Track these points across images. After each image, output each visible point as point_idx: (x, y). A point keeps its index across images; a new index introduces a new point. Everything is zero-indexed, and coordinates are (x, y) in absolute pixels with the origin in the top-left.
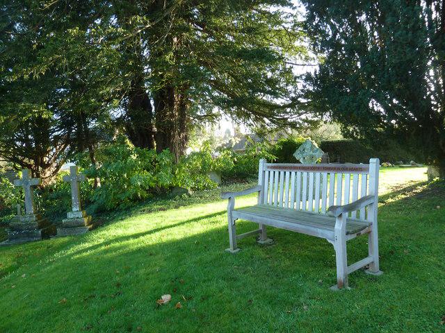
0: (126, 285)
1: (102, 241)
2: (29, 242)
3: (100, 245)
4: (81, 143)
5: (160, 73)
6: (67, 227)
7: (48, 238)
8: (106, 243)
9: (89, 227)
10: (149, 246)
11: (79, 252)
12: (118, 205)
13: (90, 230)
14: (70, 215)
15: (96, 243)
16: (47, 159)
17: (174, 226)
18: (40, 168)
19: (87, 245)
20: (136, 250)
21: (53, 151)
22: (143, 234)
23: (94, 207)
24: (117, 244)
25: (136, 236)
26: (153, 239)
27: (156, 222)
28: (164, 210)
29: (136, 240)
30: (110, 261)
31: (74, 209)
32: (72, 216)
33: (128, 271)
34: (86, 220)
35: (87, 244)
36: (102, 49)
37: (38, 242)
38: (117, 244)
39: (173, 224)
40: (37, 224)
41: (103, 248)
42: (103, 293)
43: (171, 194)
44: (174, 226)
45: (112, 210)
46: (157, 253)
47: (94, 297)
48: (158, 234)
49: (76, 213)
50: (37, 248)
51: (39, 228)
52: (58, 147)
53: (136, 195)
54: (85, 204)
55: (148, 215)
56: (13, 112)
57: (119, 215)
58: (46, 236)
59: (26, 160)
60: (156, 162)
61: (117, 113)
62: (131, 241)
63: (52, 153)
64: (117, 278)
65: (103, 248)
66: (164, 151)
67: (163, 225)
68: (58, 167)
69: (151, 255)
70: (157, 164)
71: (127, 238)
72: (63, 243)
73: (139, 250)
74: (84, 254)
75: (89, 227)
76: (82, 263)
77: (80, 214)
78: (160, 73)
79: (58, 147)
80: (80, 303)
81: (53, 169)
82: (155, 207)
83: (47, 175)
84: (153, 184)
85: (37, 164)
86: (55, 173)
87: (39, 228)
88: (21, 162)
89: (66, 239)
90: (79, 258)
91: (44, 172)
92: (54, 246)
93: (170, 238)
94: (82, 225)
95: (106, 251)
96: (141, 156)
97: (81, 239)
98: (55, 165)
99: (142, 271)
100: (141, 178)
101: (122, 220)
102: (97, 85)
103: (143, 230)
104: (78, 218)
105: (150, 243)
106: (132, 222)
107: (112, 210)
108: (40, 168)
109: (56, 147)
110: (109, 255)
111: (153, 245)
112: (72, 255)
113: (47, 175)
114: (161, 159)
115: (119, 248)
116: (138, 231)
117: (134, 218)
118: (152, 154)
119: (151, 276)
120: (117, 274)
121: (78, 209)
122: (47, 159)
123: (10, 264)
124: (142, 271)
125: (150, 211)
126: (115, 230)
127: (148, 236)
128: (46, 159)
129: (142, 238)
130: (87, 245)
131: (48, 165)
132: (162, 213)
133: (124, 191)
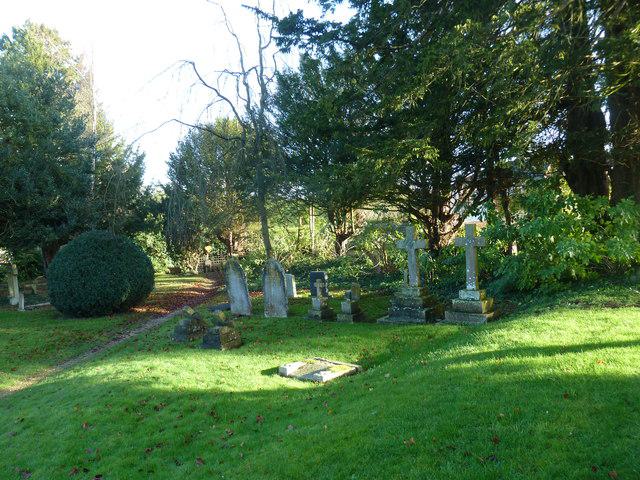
0: (508, 446)
1: (495, 347)
2: (411, 323)
3: (489, 355)
4: (493, 184)
5: (615, 64)
6: (457, 310)
7: (434, 322)
8: (500, 354)
9: (488, 316)
10: (568, 376)
11: (458, 360)
12: (538, 285)
13: (489, 320)
14: (463, 294)
15: (486, 350)
16: (448, 209)
17: (626, 344)
18: (438, 221)
19: (472, 350)
20: (534, 382)
21: (455, 197)
22: (564, 350)
23: (500, 283)
24: (516, 360)
25: (549, 351)
26: (579, 364)
27: (592, 329)
28: (614, 306)
29: (548, 359)
30: (496, 390)
31: (469, 287)
32: (466, 296)
33: (518, 417)
34: (484, 305)
35: (473, 348)
36: (507, 45)
37: (419, 326)
38: (516, 360)
39: (625, 338)
40: (421, 302)
41: (492, 361)
42: (468, 447)
43: (633, 278)
44: (626, 344)
45: (527, 291)
46: (578, 396)
47: (454, 449)
48: (590, 355)
49: (471, 292)
50: (417, 334)
51: (424, 306)
52: (462, 192)
53: (568, 272)
54: (484, 280)
55: (582, 313)
56: (391, 152)
57: (536, 303)
58: (433, 317)
59: (422, 210)
60: (606, 218)
61: (550, 136)
62: (540, 359)
63: (453, 200)
64: (498, 427)
65: (492, 361)
66: (623, 200)
67: (605, 338)
68: (461, 220)
69: (566, 396)
70: (608, 222)
71: (533, 351)
72: (450, 334)
73: (546, 381)
74: (464, 365)
75: (488, 316)
76: (457, 378)
77: (477, 295)
78: (615, 64)
79: (462, 192)
80: (430, 453)
81: (456, 222)
82: (599, 298)
83: (447, 231)
84: (598, 259)
85: (434, 216)
86: (456, 228)
87: (424, 306)
88: (416, 213)
89: (454, 329)
90: (454, 371)
91: (442, 226)
92: (437, 337)
93: (611, 368)
94: (478, 311)
95: (496, 369)
96: (583, 208)
97: (468, 336)
98: (456, 217)
99: (541, 427)
100: (576, 247)
101: (538, 313)
102: (504, 103)
103: (566, 340)
104: (473, 300)
105: (572, 371)
106: (552, 322)
107: (527, 291)
108: (438, 221)
109: (459, 192)
110: (497, 376)
111: (576, 376)
112: (449, 361)
113: (447, 231)
114: (618, 215)
115: (517, 368)
116: (557, 341)
117: (556, 313)
118: (601, 206)
119: (555, 442)
120: (499, 419)
121: (474, 287)
122: (448, 209)
123: (382, 351)
124: (541, 427)
125: (587, 306)
126: (523, 332)
127: (572, 355)
128: (446, 209)
129: (559, 357)
130: (472, 350)
131: (449, 217)
132: (608, 313)
133: (548, 265)
